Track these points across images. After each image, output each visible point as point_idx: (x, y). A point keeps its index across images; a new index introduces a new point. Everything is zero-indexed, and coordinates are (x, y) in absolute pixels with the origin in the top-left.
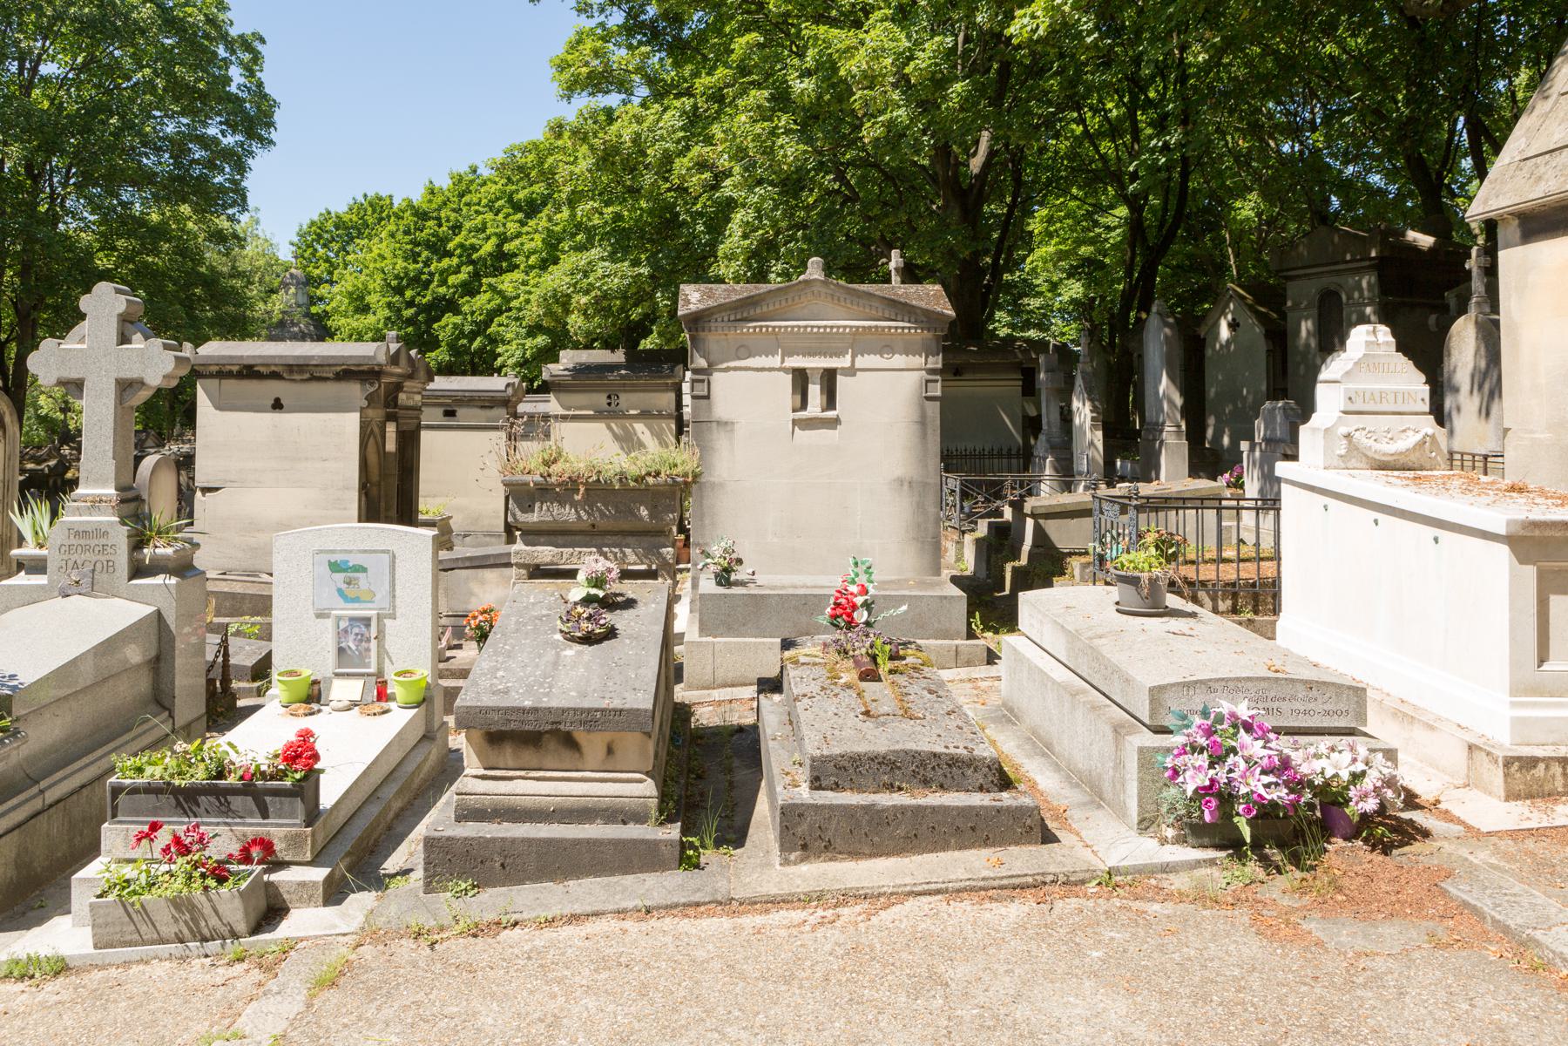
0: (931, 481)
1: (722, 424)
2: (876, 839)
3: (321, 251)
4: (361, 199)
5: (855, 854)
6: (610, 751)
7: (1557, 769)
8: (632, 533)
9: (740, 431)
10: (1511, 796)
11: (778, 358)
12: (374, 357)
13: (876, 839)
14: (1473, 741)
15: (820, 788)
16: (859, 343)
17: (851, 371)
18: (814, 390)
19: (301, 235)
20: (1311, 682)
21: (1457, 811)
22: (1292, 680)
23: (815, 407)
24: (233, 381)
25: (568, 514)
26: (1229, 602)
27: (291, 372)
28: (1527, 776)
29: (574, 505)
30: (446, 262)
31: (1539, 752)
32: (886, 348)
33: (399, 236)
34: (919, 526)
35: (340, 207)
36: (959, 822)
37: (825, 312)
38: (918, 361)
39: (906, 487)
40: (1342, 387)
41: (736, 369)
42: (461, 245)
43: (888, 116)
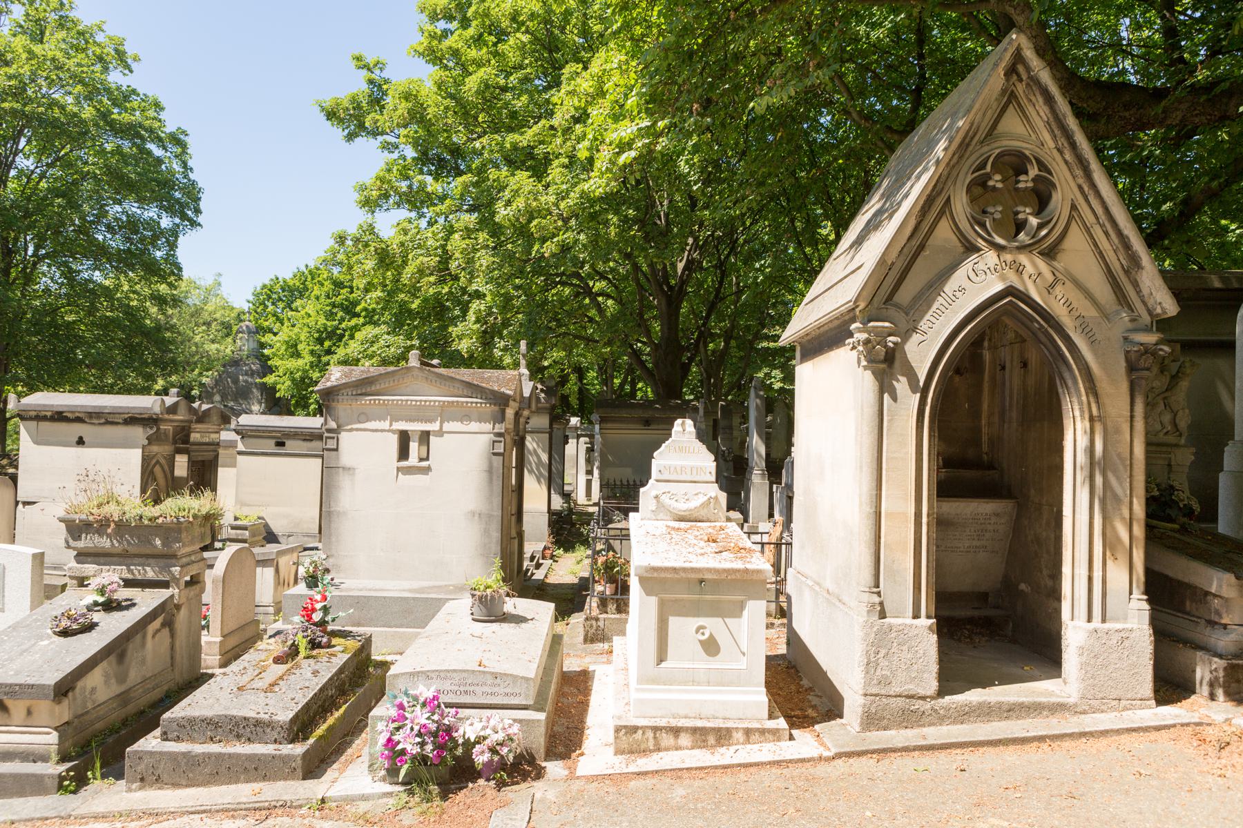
1: (346, 469)
2: (191, 775)
3: (271, 308)
4: (303, 269)
5: (176, 785)
6: (29, 712)
8: (148, 556)
10: (619, 752)
11: (388, 423)
12: (151, 409)
13: (191, 775)
15: (167, 740)
16: (445, 413)
17: (440, 433)
19: (256, 295)
24: (47, 423)
25: (104, 543)
27: (91, 417)
29: (109, 536)
30: (354, 321)
32: (466, 417)
33: (322, 300)
35: (287, 274)
36: (247, 764)
37: (424, 392)
38: (488, 427)
41: (357, 430)
42: (365, 309)
43: (560, 238)
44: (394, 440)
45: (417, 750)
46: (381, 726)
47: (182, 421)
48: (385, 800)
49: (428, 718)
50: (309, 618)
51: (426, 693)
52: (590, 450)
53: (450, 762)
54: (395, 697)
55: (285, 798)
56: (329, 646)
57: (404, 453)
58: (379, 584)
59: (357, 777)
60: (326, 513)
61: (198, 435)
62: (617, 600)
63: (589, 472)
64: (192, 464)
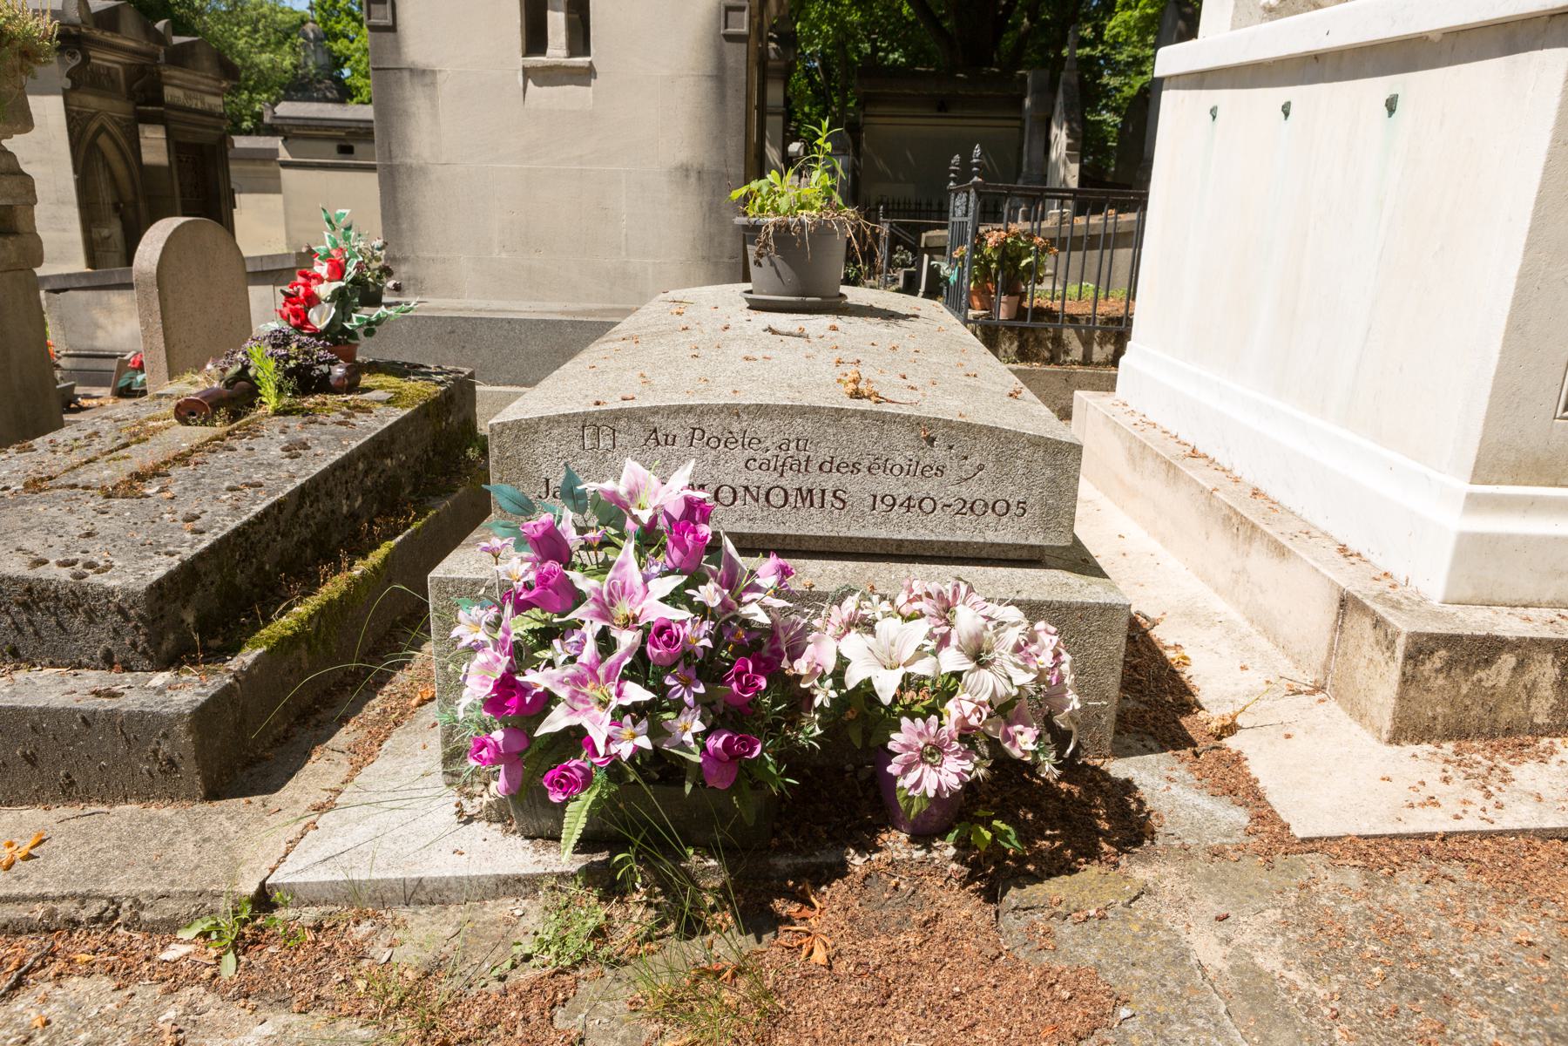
1: (422, 74)
7: (1546, 671)
9: (445, 86)
20: (931, 423)
21: (1259, 767)
22: (881, 419)
23: (557, 50)
26: (1110, 349)
28: (1462, 687)
31: (1509, 625)
34: (711, 239)
39: (693, 179)
45: (632, 742)
46: (470, 625)
47: (134, 52)
48: (508, 907)
49: (673, 599)
50: (302, 323)
51: (659, 490)
53: (781, 781)
54: (527, 508)
55: (112, 887)
56: (352, 386)
59: (392, 814)
61: (179, 93)
64: (175, 146)
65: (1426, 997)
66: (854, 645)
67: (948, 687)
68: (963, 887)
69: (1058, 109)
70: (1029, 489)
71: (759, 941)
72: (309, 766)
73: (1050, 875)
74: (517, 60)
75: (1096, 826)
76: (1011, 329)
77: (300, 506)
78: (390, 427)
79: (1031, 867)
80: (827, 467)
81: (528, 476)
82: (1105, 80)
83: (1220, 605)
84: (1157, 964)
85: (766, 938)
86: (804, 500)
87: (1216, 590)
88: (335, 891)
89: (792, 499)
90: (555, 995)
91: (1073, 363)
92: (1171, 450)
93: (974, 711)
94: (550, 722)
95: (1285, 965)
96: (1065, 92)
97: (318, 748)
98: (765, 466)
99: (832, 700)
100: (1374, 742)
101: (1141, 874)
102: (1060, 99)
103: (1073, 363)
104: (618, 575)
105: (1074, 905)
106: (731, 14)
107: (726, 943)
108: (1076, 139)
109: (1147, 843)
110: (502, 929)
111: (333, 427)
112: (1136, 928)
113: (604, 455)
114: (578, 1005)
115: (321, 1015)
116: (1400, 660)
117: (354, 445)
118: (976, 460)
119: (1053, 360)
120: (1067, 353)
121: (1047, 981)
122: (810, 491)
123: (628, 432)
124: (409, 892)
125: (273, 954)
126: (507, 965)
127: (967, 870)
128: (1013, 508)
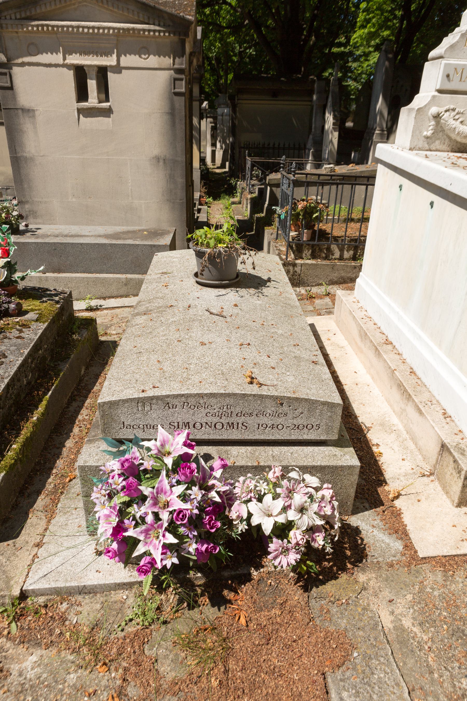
0: (179, 159)
1: (29, 112)
9: (40, 118)
11: (61, 55)
14: (449, 441)
16: (124, 44)
17: (118, 69)
18: (92, 84)
20: (282, 398)
26: (351, 252)
32: (143, 50)
38: (167, 61)
39: (161, 163)
40: (444, 62)
41: (30, 64)
44: (69, 77)
48: (122, 595)
52: (214, 129)
56: (20, 312)
57: (82, 95)
58: (74, 229)
60: (17, 161)
62: (313, 246)
63: (214, 145)
65: (462, 638)
66: (253, 506)
67: (289, 525)
68: (295, 584)
69: (329, 104)
70: (321, 420)
71: (219, 610)
72: (29, 521)
73: (328, 580)
74: (74, 105)
75: (345, 553)
76: (308, 245)
77: (8, 392)
78: (40, 337)
79: (321, 577)
80: (239, 414)
81: (115, 421)
82: (350, 64)
83: (395, 420)
84: (367, 629)
85: (222, 608)
86: (230, 427)
87: (394, 411)
88: (51, 591)
89: (225, 427)
90: (144, 639)
91: (335, 259)
92: (378, 339)
93: (301, 539)
94: (137, 550)
95: (413, 624)
96: (332, 96)
97: (31, 510)
98: (214, 415)
99: (246, 529)
100: (451, 506)
101: (362, 577)
102: (330, 99)
103: (335, 259)
104: (160, 485)
105: (337, 597)
106: (176, 82)
107: (208, 612)
108: (337, 120)
109: (364, 560)
110: (119, 605)
111: (14, 340)
112: (360, 610)
113: (147, 413)
114: (153, 643)
115: (54, 651)
116: (462, 480)
117: (26, 352)
118: (300, 410)
119: (326, 258)
120: (333, 255)
121: (328, 635)
122: (233, 423)
123: (157, 404)
124: (80, 590)
125: (30, 621)
126: (123, 623)
127: (297, 576)
128: (315, 427)
